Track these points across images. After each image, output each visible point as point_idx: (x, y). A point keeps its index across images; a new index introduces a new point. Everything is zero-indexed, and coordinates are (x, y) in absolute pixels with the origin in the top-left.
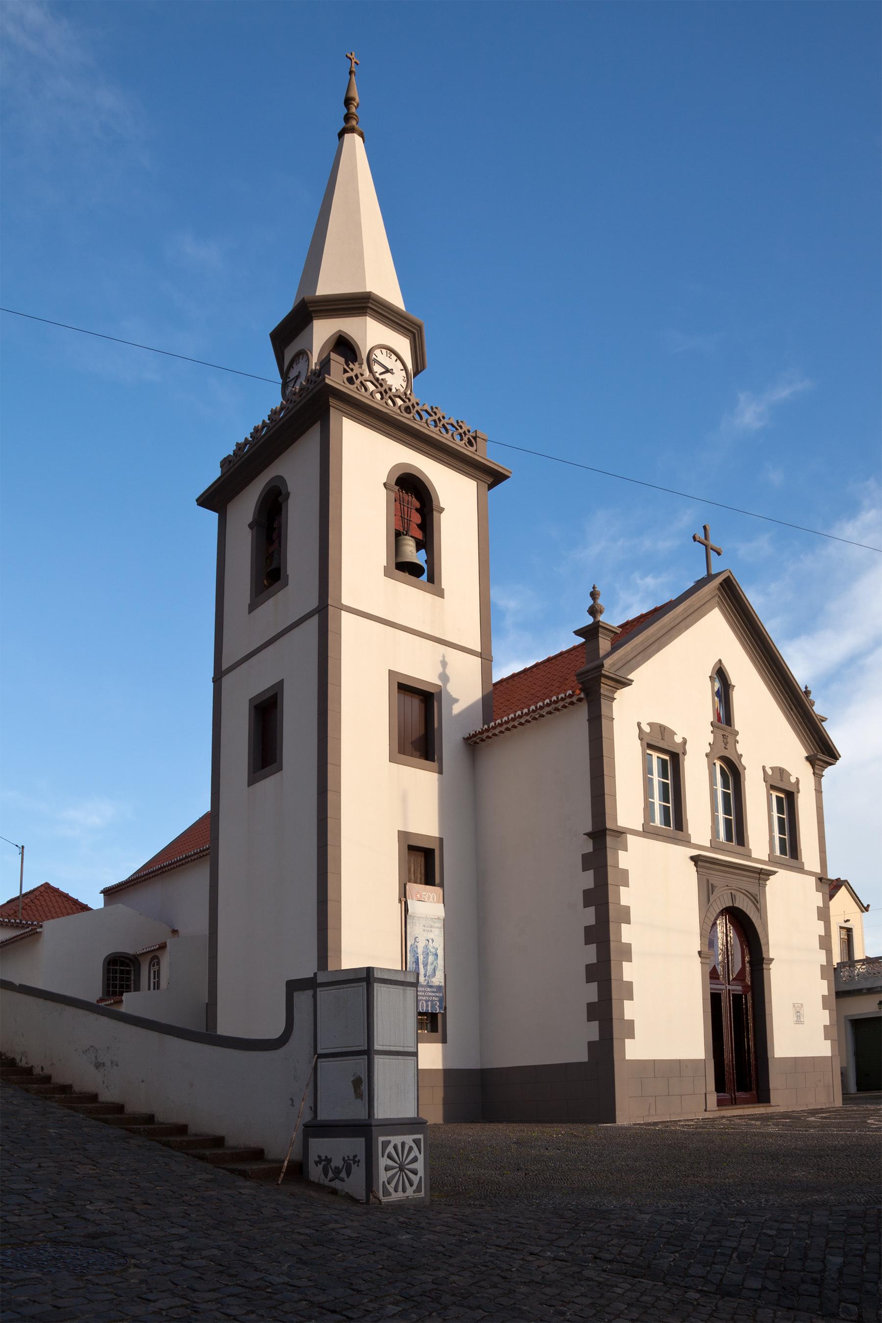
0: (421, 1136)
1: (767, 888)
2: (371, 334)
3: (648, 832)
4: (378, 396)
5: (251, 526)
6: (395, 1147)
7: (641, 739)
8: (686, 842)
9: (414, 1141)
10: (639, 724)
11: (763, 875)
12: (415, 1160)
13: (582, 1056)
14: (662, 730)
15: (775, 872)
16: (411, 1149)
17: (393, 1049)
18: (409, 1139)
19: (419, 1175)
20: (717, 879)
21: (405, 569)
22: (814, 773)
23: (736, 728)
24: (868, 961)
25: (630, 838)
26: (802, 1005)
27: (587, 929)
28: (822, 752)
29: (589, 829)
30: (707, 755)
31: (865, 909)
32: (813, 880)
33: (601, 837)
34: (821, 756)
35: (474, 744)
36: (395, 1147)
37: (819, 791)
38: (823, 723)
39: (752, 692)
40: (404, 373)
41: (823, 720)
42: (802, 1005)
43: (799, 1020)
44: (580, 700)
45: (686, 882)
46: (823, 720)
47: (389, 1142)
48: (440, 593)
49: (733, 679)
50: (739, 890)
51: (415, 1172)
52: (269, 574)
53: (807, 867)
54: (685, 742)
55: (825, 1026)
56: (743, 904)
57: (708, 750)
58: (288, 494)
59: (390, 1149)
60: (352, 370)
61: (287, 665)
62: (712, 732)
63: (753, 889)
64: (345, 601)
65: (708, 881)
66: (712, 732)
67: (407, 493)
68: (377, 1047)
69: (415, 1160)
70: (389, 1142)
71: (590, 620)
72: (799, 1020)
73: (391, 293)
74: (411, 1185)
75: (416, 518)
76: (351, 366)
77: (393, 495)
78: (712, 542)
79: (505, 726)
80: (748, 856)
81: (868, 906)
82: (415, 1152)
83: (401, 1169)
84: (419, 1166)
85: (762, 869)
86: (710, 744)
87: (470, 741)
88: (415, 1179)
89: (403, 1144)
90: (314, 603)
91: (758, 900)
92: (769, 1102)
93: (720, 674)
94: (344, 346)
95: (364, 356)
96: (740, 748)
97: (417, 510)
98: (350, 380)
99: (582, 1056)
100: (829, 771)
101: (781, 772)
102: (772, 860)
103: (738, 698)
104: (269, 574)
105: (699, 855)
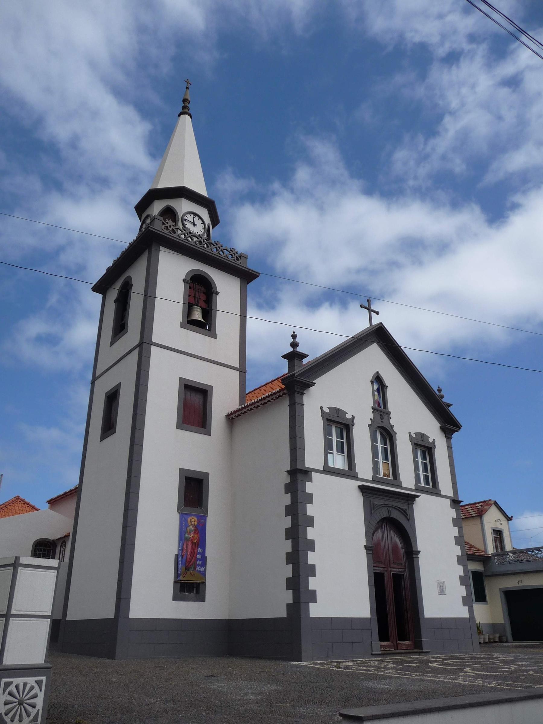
0: (44, 678)
1: (415, 506)
2: (183, 206)
3: (328, 471)
4: (183, 236)
5: (115, 301)
6: (17, 687)
7: (322, 416)
8: (354, 477)
9: (36, 682)
10: (321, 408)
11: (410, 499)
12: (35, 696)
13: (283, 614)
14: (337, 411)
15: (418, 496)
16: (32, 688)
17: (37, 613)
18: (31, 681)
19: (37, 708)
20: (378, 502)
21: (190, 323)
22: (446, 437)
23: (389, 410)
24: (516, 552)
25: (314, 474)
26: (444, 582)
27: (287, 530)
28: (449, 425)
29: (288, 468)
30: (369, 426)
31: (509, 519)
32: (448, 501)
33: (298, 474)
34: (448, 426)
35: (232, 418)
36: (17, 687)
37: (449, 447)
38: (450, 408)
39: (399, 390)
40: (203, 225)
41: (449, 405)
42: (444, 582)
43: (442, 592)
44: (284, 394)
45: (357, 503)
46: (449, 405)
47: (12, 683)
48: (215, 336)
49: (387, 382)
50: (394, 508)
51: (34, 706)
52: (120, 327)
53: (442, 493)
54: (353, 417)
55: (463, 597)
56: (395, 515)
57: (370, 422)
58: (132, 285)
59: (12, 688)
60: (168, 223)
61: (125, 376)
62: (373, 412)
63: (403, 506)
64: (154, 340)
65: (370, 501)
66: (373, 412)
67: (198, 284)
68: (13, 612)
69: (35, 696)
70: (12, 683)
71: (292, 349)
72: (442, 592)
73: (201, 190)
74: (28, 716)
75: (203, 297)
76: (167, 221)
77: (188, 286)
78: (372, 308)
79: (247, 409)
80: (400, 486)
81: (512, 517)
82: (36, 690)
83: (21, 703)
84: (39, 702)
85: (408, 494)
86: (371, 419)
87: (230, 417)
88: (33, 712)
89: (25, 684)
90: (137, 342)
91: (409, 515)
92: (421, 648)
93: (378, 379)
94: (169, 213)
95: (180, 217)
96: (392, 422)
97: (204, 293)
98: (167, 228)
99: (283, 614)
100: (455, 435)
101: (422, 436)
102: (418, 489)
103: (390, 393)
104: (120, 327)
105: (363, 485)
